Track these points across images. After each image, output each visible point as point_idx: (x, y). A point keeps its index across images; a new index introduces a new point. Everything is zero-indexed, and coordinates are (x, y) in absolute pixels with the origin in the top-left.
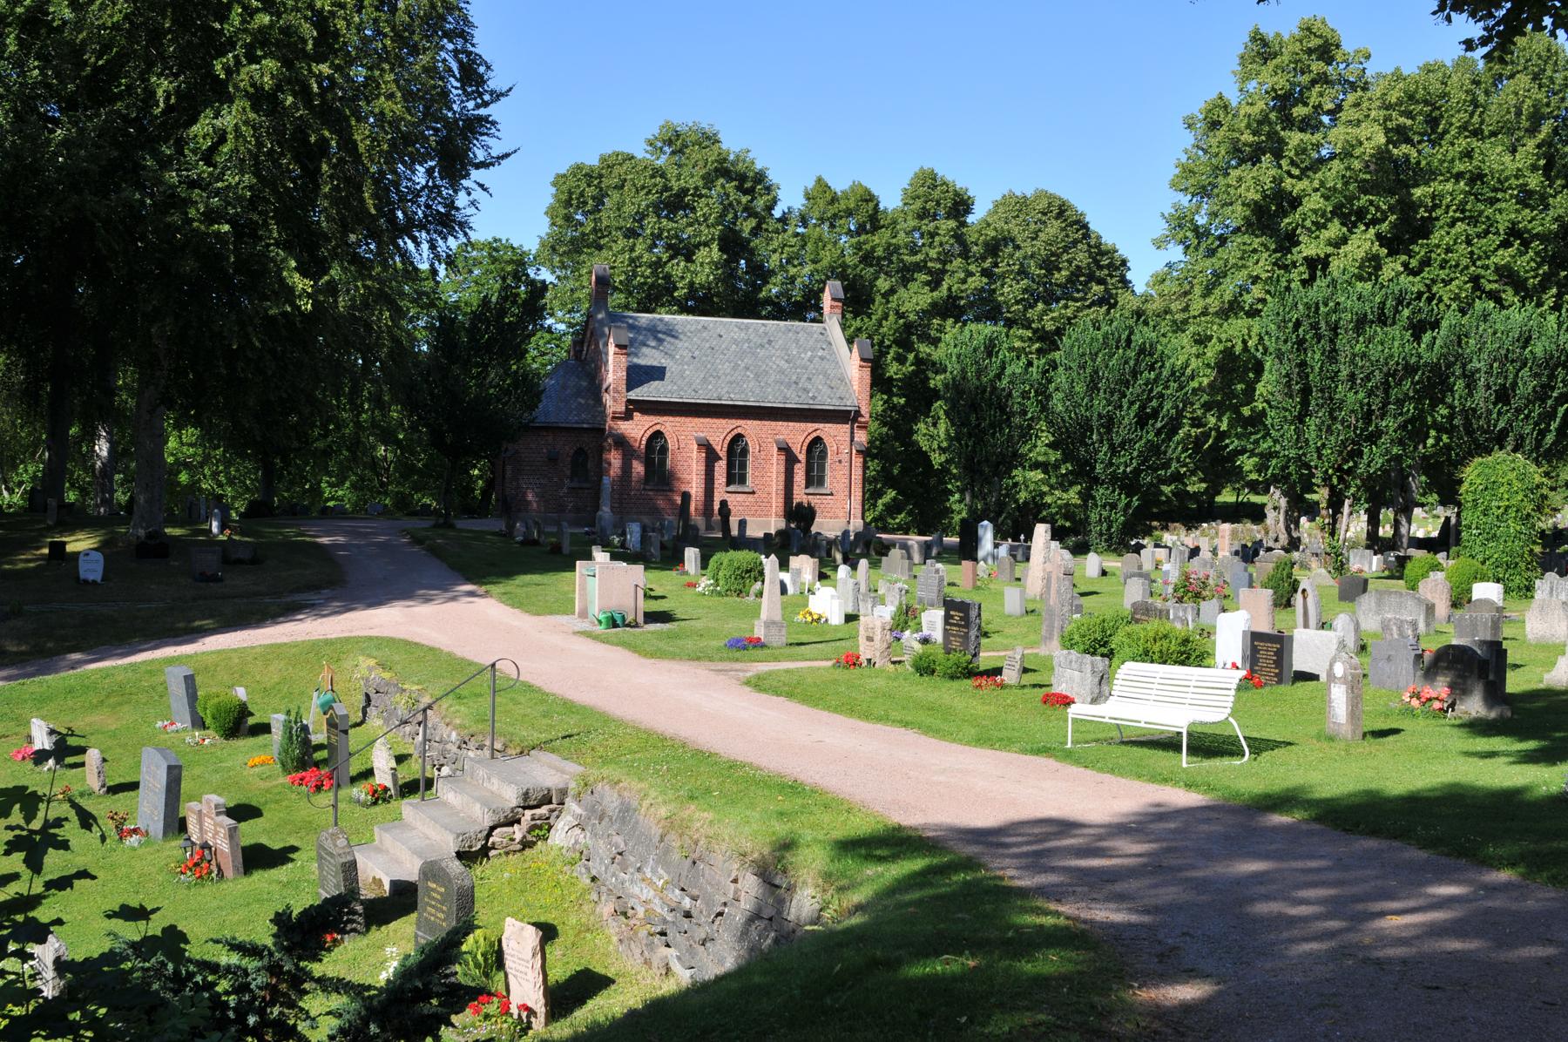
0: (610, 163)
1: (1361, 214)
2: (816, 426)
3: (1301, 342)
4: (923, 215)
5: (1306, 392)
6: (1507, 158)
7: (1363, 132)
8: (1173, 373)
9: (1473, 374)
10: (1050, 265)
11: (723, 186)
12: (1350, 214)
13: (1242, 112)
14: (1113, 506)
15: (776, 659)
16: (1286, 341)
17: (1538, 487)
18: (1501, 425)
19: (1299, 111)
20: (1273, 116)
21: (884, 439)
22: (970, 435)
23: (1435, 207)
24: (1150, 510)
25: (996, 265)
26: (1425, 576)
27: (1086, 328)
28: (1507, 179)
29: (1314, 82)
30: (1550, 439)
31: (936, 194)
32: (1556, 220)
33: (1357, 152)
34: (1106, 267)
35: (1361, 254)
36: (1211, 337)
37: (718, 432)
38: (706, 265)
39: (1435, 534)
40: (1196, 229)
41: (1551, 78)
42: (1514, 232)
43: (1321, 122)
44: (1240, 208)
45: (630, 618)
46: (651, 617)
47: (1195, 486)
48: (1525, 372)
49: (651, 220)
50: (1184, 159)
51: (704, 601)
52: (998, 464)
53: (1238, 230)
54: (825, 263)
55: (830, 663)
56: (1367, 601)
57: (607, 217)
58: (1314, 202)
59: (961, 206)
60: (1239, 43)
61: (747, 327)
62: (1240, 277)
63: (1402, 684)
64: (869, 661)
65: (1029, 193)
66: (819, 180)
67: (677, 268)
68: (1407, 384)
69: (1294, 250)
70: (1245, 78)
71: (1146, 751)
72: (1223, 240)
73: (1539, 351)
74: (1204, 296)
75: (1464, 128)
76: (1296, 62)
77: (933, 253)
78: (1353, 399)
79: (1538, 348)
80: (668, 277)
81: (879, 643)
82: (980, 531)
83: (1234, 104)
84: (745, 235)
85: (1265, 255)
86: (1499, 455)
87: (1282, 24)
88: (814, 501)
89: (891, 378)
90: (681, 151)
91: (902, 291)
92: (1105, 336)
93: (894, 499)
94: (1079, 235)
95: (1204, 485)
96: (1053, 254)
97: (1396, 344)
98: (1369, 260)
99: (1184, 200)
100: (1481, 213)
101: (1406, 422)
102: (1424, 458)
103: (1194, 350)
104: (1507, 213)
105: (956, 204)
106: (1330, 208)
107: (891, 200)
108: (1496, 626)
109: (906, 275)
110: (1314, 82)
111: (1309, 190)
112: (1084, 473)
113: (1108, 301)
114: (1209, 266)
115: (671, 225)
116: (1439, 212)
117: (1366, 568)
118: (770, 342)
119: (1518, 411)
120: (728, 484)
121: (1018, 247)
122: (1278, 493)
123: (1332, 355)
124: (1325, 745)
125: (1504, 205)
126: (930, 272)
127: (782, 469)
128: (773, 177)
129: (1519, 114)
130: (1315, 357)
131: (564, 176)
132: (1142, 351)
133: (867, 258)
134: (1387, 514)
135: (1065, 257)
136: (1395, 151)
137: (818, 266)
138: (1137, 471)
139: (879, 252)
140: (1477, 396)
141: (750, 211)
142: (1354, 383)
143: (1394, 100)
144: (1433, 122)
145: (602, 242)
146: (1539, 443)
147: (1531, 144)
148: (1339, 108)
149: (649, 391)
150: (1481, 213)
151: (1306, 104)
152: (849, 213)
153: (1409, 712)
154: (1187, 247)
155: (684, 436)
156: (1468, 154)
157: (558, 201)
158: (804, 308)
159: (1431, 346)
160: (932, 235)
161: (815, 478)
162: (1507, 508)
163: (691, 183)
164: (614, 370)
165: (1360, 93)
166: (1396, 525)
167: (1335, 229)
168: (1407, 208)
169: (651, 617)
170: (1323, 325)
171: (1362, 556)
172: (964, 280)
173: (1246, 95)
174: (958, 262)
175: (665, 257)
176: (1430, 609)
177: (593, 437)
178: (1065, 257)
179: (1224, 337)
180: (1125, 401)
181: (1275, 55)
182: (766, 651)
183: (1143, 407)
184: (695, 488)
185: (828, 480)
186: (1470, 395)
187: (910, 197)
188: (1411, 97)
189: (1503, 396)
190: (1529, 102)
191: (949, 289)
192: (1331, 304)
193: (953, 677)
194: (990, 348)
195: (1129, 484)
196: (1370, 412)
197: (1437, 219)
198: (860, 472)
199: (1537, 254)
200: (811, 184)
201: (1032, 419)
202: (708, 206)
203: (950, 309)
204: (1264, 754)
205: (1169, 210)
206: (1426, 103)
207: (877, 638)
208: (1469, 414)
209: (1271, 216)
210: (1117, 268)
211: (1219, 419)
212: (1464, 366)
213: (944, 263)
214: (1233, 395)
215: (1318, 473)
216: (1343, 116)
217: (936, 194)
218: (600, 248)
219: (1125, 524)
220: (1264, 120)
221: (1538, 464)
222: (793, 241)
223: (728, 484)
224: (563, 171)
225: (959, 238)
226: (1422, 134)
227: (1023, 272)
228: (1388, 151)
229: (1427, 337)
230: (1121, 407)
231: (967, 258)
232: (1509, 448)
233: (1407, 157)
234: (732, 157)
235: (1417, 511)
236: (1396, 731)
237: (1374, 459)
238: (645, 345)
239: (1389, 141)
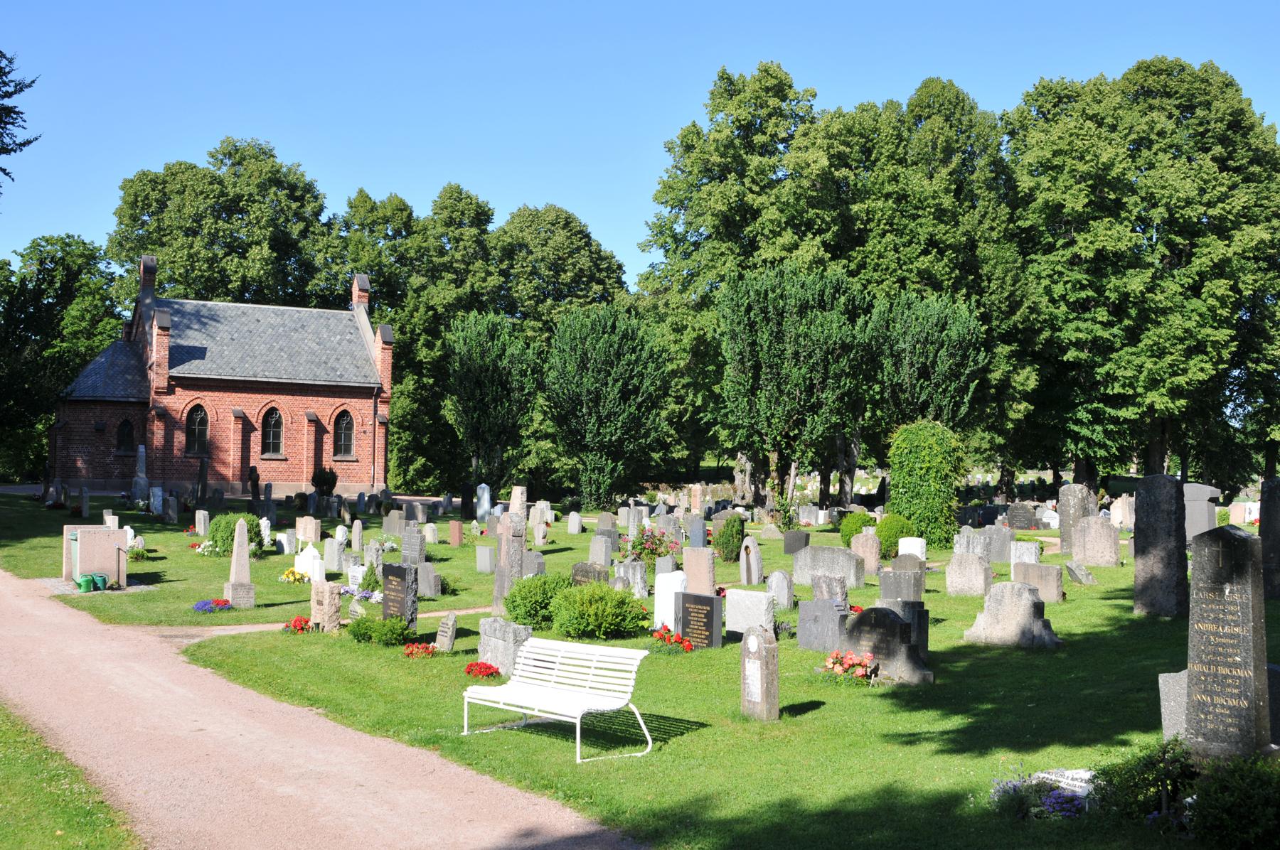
0: (173, 172)
1: (809, 225)
2: (343, 400)
3: (752, 325)
4: (450, 223)
5: (757, 368)
6: (926, 182)
7: (810, 156)
8: (651, 356)
9: (899, 354)
10: (557, 268)
11: (276, 194)
12: (800, 225)
13: (711, 137)
14: (601, 470)
15: (239, 623)
16: (739, 323)
17: (954, 450)
18: (923, 397)
19: (759, 139)
20: (737, 142)
21: (414, 414)
22: (475, 409)
23: (869, 220)
24: (638, 473)
25: (512, 267)
26: (858, 531)
27: (571, 315)
28: (926, 199)
29: (770, 115)
30: (964, 410)
31: (461, 205)
32: (964, 234)
33: (806, 172)
34: (604, 271)
35: (809, 257)
36: (686, 327)
37: (254, 406)
38: (258, 260)
39: (874, 491)
40: (675, 237)
41: (959, 120)
42: (932, 243)
43: (777, 149)
44: (710, 218)
45: (111, 581)
46: (134, 579)
47: (680, 453)
48: (943, 352)
49: (208, 221)
50: (665, 177)
51: (200, 562)
52: (500, 433)
53: (709, 237)
54: (364, 261)
55: (282, 626)
56: (804, 555)
57: (168, 217)
58: (771, 214)
59: (482, 217)
60: (709, 81)
61: (283, 313)
62: (711, 275)
63: (827, 647)
64: (318, 625)
66: (361, 192)
68: (844, 362)
69: (755, 254)
70: (716, 109)
71: (543, 740)
72: (697, 245)
73: (954, 335)
74: (681, 292)
75: (891, 157)
76: (757, 98)
77: (458, 256)
78: (796, 373)
79: (954, 332)
80: (223, 271)
81: (327, 609)
82: (479, 492)
83: (705, 131)
85: (731, 258)
86: (921, 422)
87: (745, 69)
88: (338, 468)
89: (421, 361)
90: (239, 163)
91: (431, 288)
92: (593, 324)
93: (424, 465)
94: (582, 243)
95: (687, 453)
96: (560, 258)
97: (835, 326)
98: (816, 263)
99: (665, 211)
100: (906, 226)
101: (843, 395)
102: (863, 428)
103: (672, 338)
104: (926, 227)
105: (478, 214)
106: (784, 220)
107: (422, 210)
108: (918, 583)
109: (434, 274)
110: (770, 115)
111: (767, 204)
112: (575, 445)
113: (606, 297)
114: (685, 267)
115: (227, 226)
116: (872, 225)
117: (813, 522)
118: (303, 327)
119: (937, 385)
120: (263, 453)
121: (531, 253)
122: (744, 458)
123: (779, 337)
124: (738, 725)
125: (923, 220)
126: (456, 272)
127: (312, 438)
128: (321, 188)
129: (934, 148)
130: (764, 337)
131: (132, 181)
132: (625, 336)
133: (402, 259)
134: (834, 476)
135: (570, 261)
136: (837, 173)
137: (358, 265)
138: (621, 441)
139: (412, 254)
140: (902, 373)
141: (299, 216)
142: (798, 360)
143: (835, 131)
144: (867, 151)
145: (165, 239)
146: (955, 412)
147: (944, 172)
148: (792, 137)
149: (189, 369)
150: (906, 226)
151: (764, 133)
152: (386, 220)
153: (832, 679)
154: (667, 251)
155: (223, 412)
156: (894, 179)
157: (125, 202)
158: (342, 301)
159: (863, 330)
160: (458, 240)
161: (342, 447)
162: (929, 468)
163: (246, 191)
164: (158, 349)
165: (808, 125)
166: (842, 482)
167: (788, 237)
168: (846, 220)
169: (134, 579)
170: (771, 308)
171: (810, 512)
172: (484, 279)
173: (716, 125)
174: (479, 263)
175: (220, 253)
176: (860, 564)
177: (136, 411)
178: (570, 261)
179: (697, 326)
180: (610, 379)
181: (740, 92)
182: (233, 614)
183: (625, 384)
185: (354, 448)
186: (897, 371)
187: (439, 207)
188: (850, 131)
189: (924, 373)
190: (942, 138)
191: (472, 286)
192: (778, 291)
193: (387, 644)
194: (493, 333)
195: (614, 451)
196: (812, 386)
197: (871, 230)
198: (383, 441)
199: (950, 260)
200: (354, 195)
201: (529, 394)
202: (260, 211)
203: (473, 302)
204: (673, 741)
205: (652, 220)
206: (862, 136)
207: (326, 602)
208: (897, 388)
209: (735, 225)
210: (614, 271)
211: (695, 395)
212: (891, 348)
213: (468, 264)
214: (705, 374)
215: (768, 439)
216: (794, 143)
217: (461, 205)
218: (163, 245)
219: (611, 485)
220: (731, 144)
221: (955, 432)
222: (336, 242)
223: (263, 453)
224: (130, 176)
225: (480, 243)
226: (860, 161)
227: (535, 272)
228: (831, 173)
229: (860, 321)
230: (606, 384)
231: (487, 260)
232: (930, 417)
233: (846, 178)
234: (284, 170)
235: (859, 473)
236: (815, 705)
237: (816, 426)
238: (189, 327)
239: (831, 165)
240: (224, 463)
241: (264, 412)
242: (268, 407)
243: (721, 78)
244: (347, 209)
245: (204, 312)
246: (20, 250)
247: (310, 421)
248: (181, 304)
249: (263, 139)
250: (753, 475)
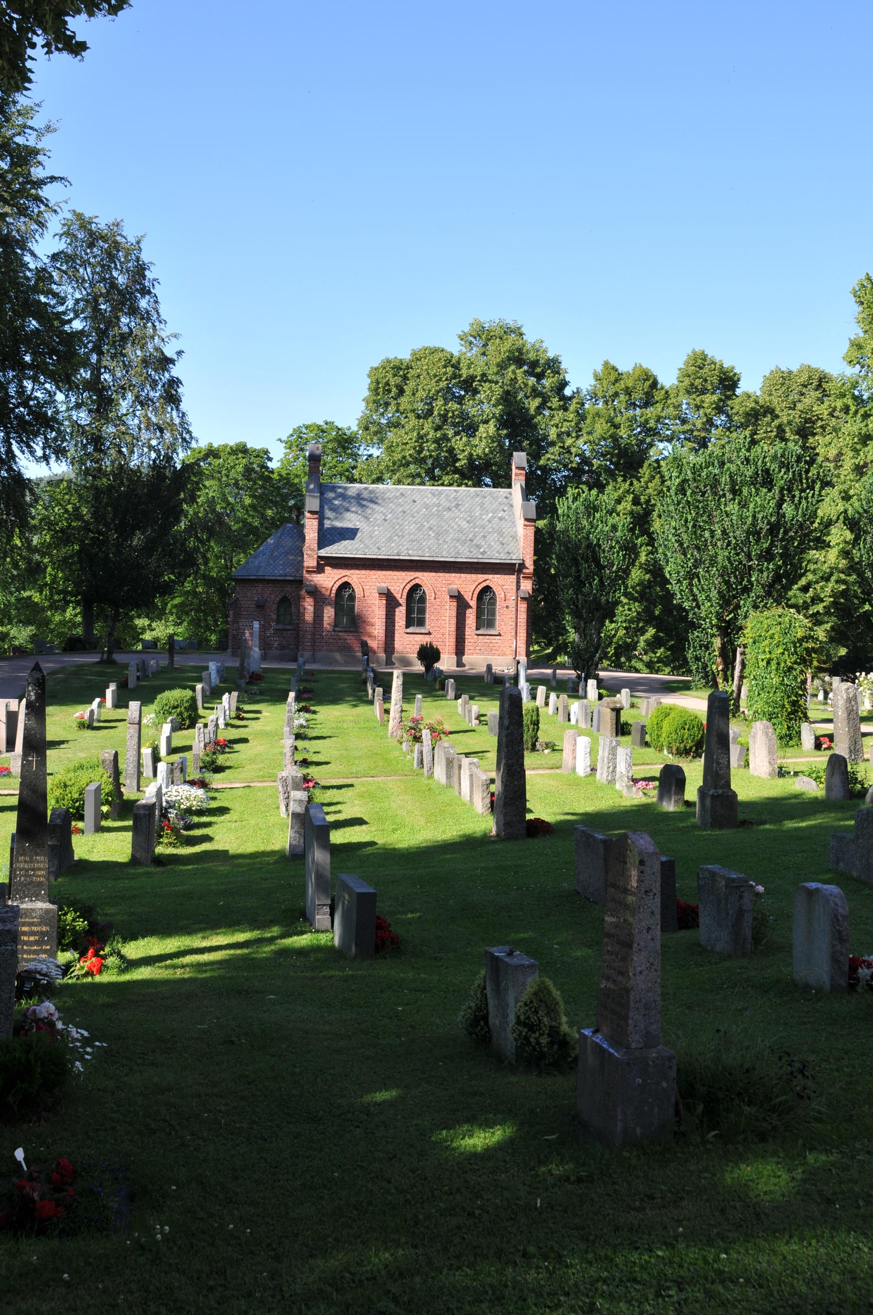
2: (486, 576)
11: (514, 372)
37: (398, 583)
59: (728, 382)
61: (440, 493)
65: (795, 368)
66: (606, 364)
67: (459, 443)
80: (451, 450)
84: (532, 412)
93: (655, 636)
105: (721, 381)
107: (668, 378)
118: (457, 506)
120: (407, 627)
121: (777, 417)
127: (454, 613)
155: (368, 587)
184: (378, 629)
200: (599, 368)
223: (407, 627)
224: (376, 365)
238: (348, 510)
240: (370, 636)
241: (408, 588)
242: (412, 584)
244: (593, 382)
245: (365, 495)
246: (284, 438)
247: (451, 597)
248: (346, 489)
249: (510, 320)
250: (312, 694)
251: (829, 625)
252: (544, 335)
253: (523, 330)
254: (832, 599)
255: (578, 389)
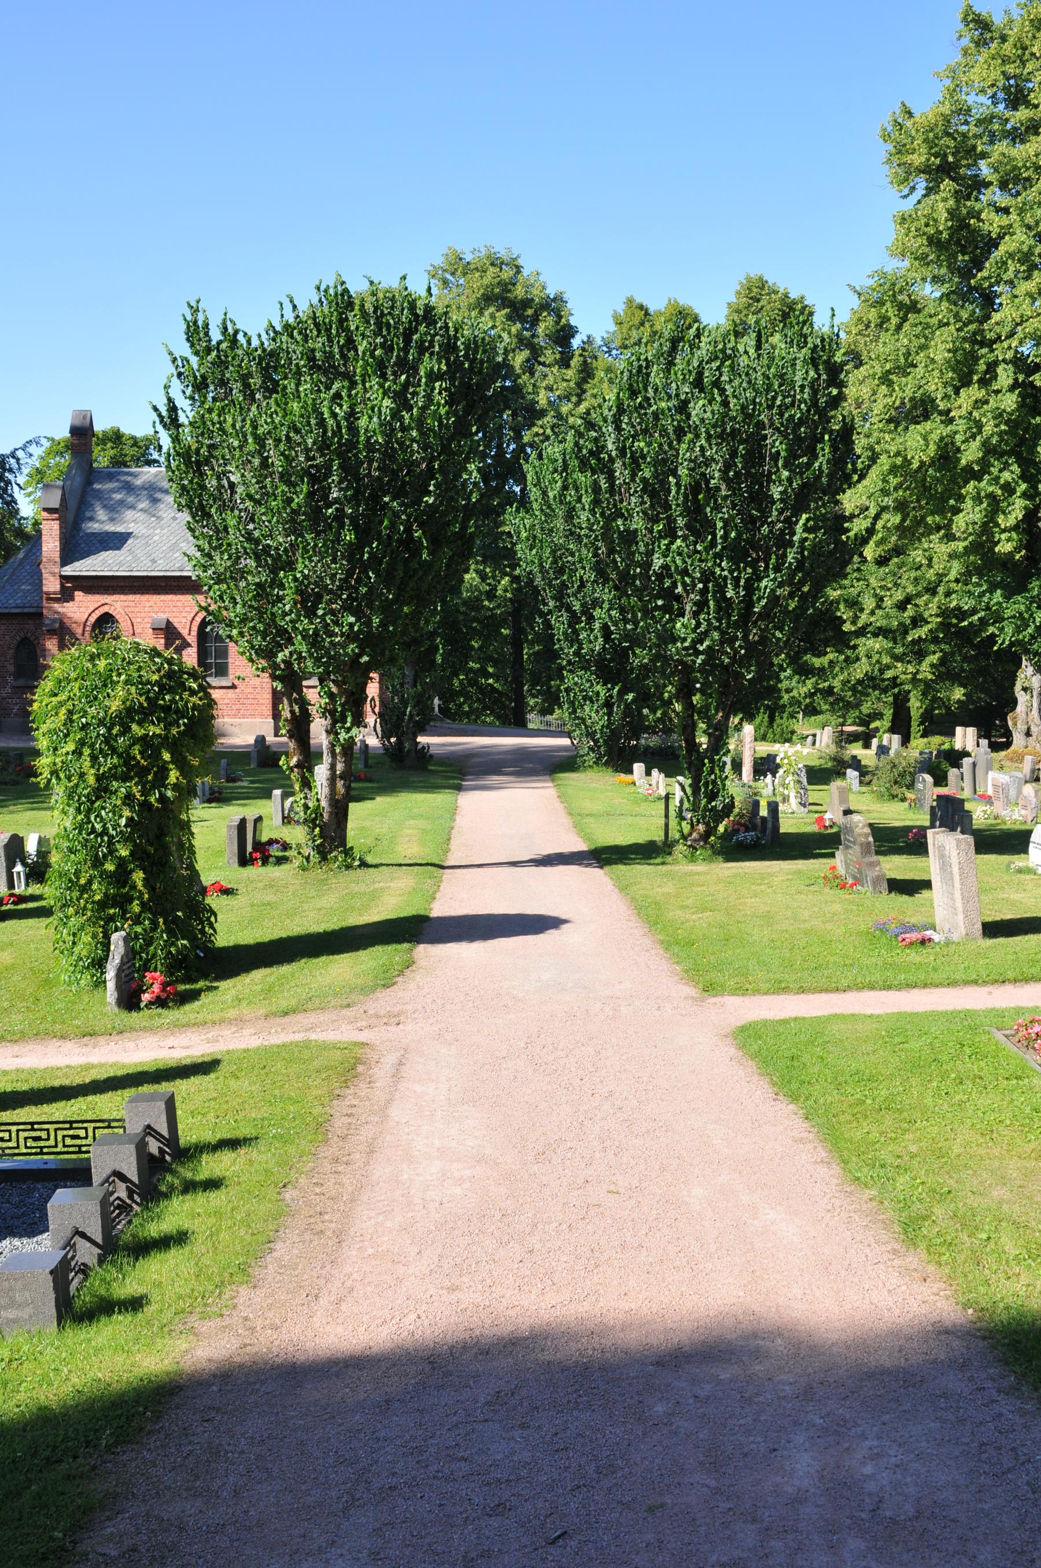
66: (630, 301)
200: (621, 308)
243: (966, 21)
244: (613, 328)
251: (938, 655)
252: (547, 272)
253: (520, 262)
254: (939, 620)
255: (589, 337)
